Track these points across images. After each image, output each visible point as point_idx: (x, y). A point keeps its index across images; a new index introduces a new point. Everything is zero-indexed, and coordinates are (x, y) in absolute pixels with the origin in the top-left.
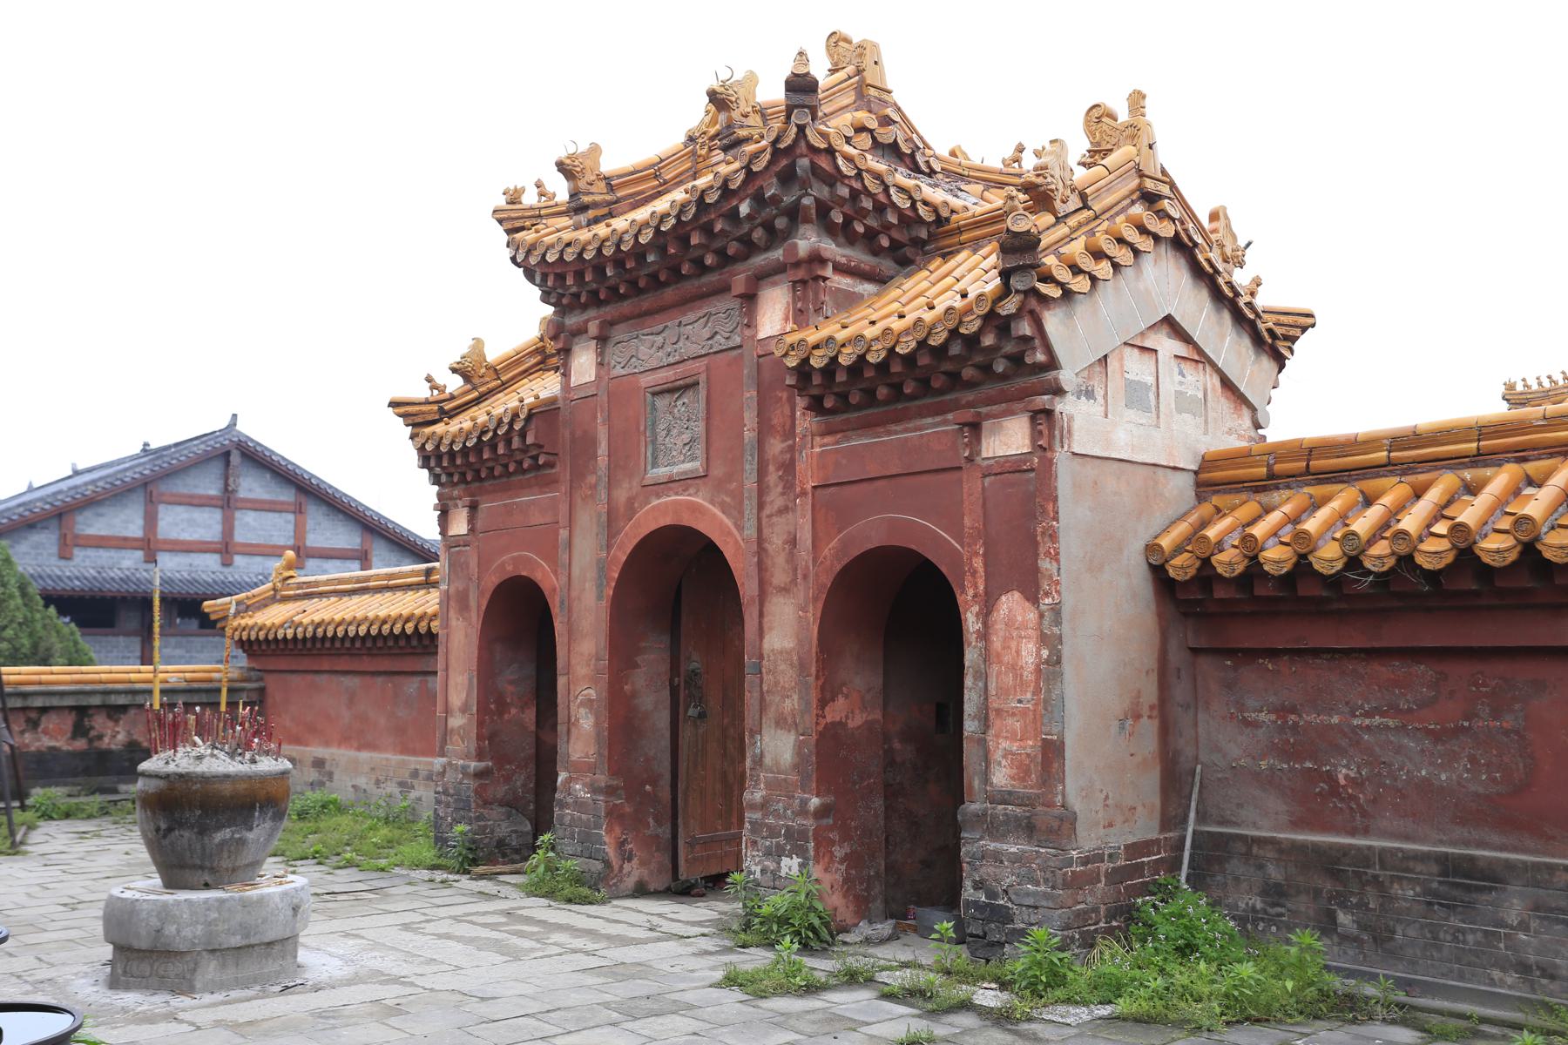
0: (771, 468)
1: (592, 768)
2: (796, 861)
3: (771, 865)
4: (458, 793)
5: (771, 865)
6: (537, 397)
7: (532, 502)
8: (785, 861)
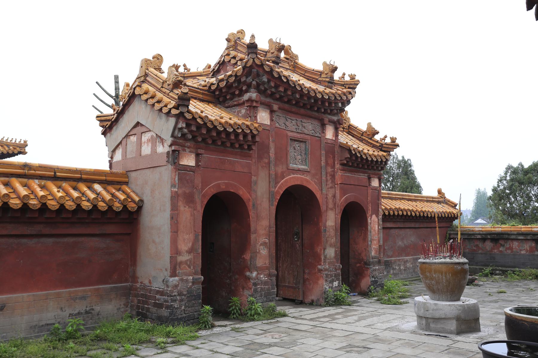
0: (328, 175)
1: (268, 268)
2: (337, 282)
3: (331, 285)
4: (188, 292)
5: (331, 285)
6: (347, 143)
7: (237, 162)
8: (334, 283)
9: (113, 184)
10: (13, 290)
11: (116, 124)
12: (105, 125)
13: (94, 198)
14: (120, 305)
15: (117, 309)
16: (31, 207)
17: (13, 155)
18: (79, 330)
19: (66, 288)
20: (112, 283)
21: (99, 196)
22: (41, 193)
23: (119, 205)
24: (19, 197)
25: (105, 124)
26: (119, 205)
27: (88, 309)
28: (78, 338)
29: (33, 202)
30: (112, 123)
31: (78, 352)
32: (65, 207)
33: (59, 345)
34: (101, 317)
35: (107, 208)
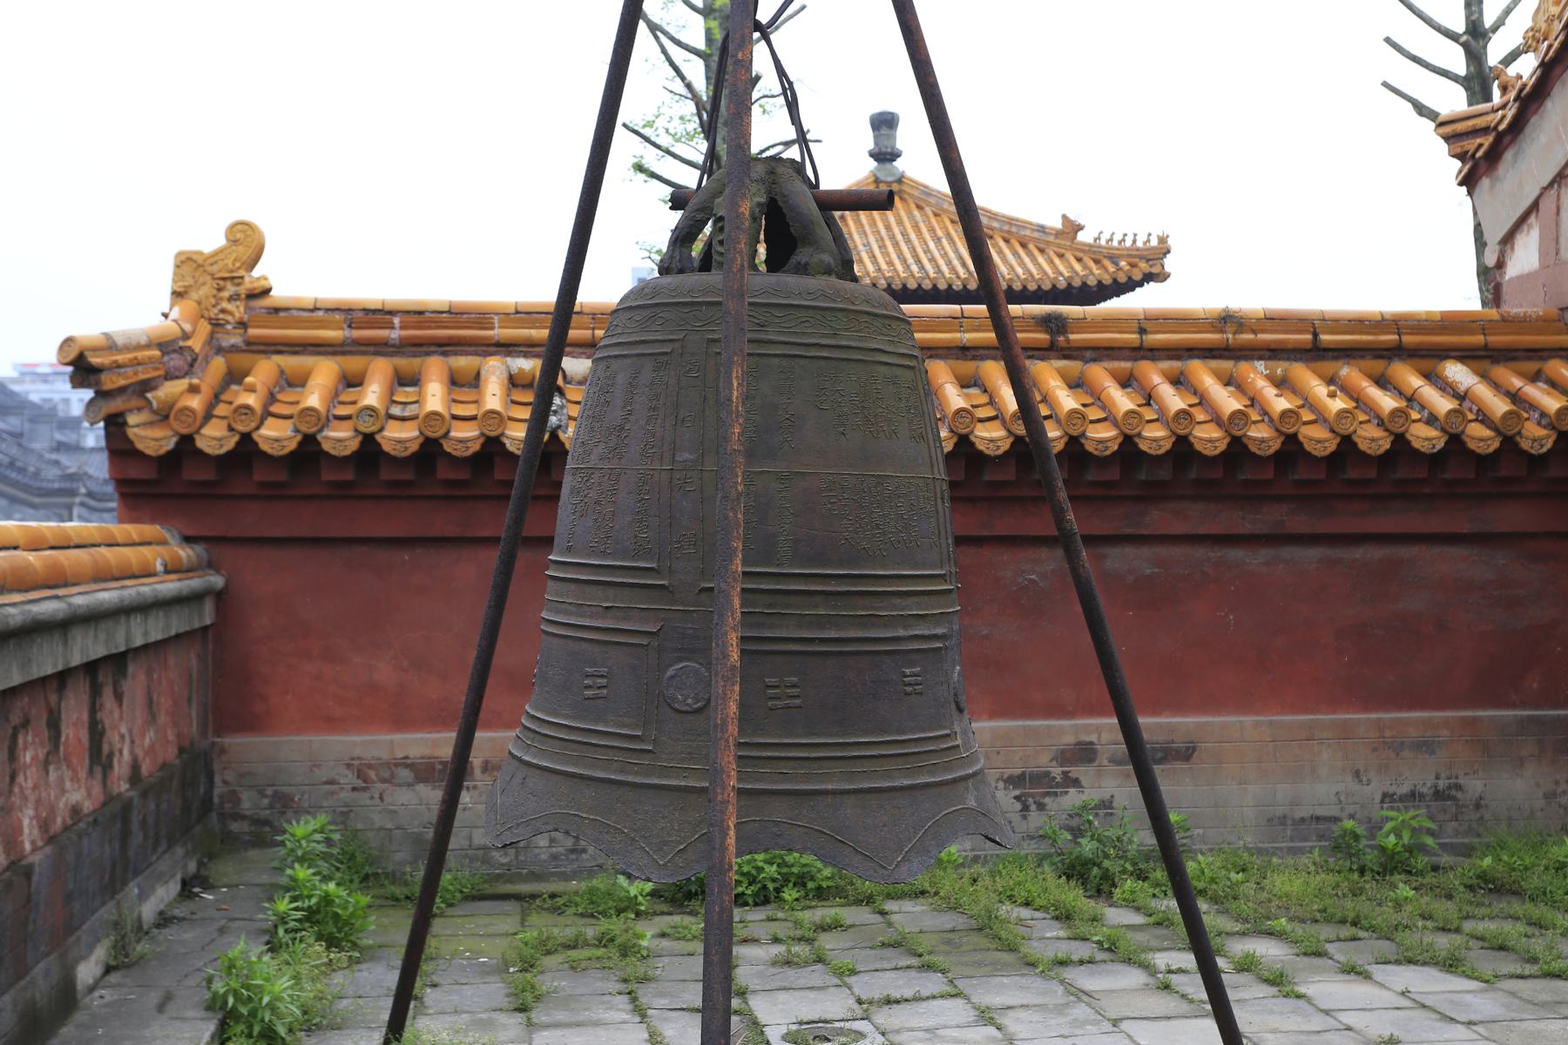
9: (1513, 359)
10: (1212, 703)
11: (1513, 141)
12: (1472, 148)
13: (1450, 412)
14: (1557, 783)
15: (1546, 796)
16: (1253, 449)
17: (1130, 286)
18: (1423, 849)
19: (1366, 709)
20: (1523, 705)
21: (1467, 404)
22: (1281, 404)
23: (1543, 432)
24: (1217, 419)
25: (1470, 145)
26: (1542, 432)
27: (1442, 784)
28: (1421, 873)
29: (1259, 433)
30: (1500, 137)
31: (1430, 917)
32: (1355, 444)
33: (1370, 886)
34: (1487, 816)
35: (1496, 445)
